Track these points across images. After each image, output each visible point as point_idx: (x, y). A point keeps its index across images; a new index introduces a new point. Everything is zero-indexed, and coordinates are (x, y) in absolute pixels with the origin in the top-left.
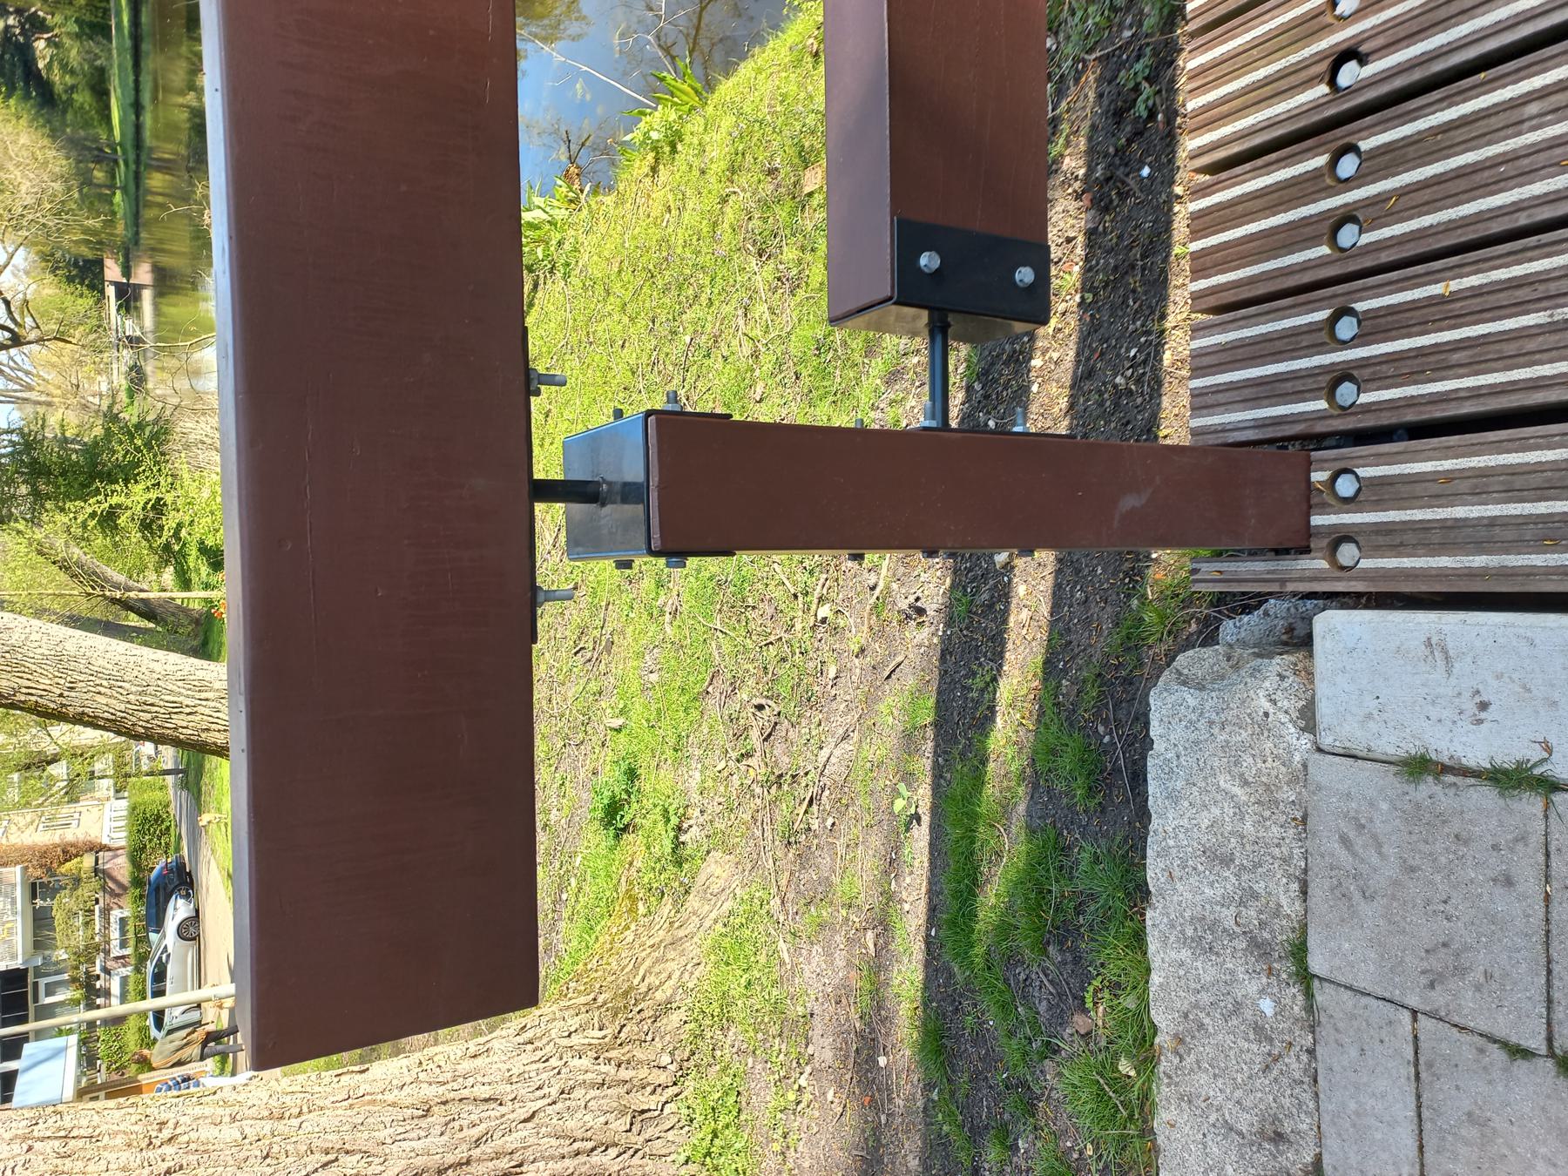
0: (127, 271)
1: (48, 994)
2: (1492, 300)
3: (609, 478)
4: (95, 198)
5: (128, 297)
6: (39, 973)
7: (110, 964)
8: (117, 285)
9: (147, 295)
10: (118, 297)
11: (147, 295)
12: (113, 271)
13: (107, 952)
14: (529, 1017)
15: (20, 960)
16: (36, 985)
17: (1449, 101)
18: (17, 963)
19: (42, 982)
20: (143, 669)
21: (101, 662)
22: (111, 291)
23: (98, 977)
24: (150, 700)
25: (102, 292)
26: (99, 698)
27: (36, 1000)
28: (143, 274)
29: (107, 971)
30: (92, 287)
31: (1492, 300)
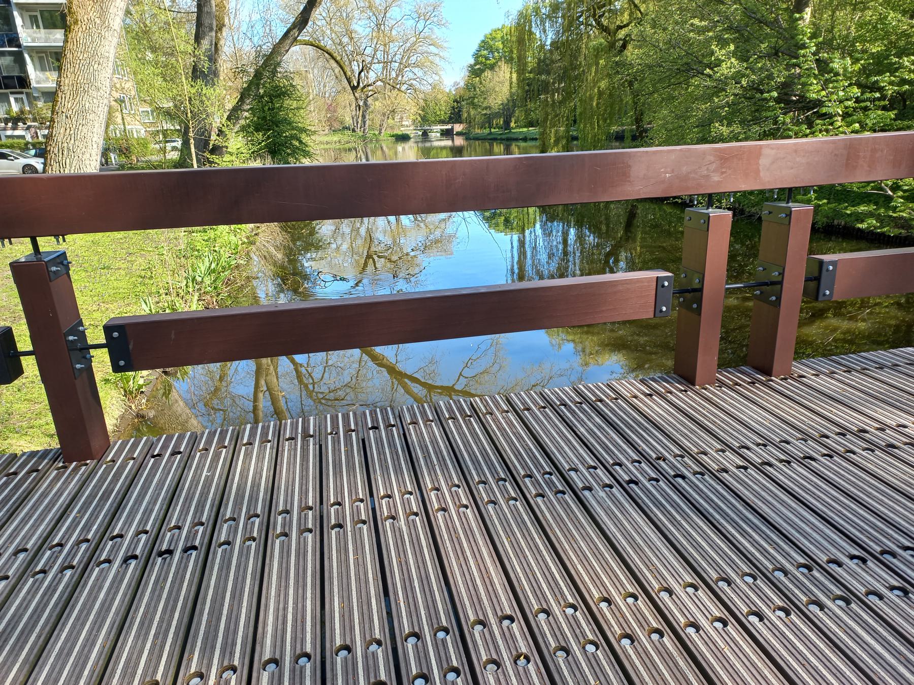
0: (459, 134)
1: (16, 99)
2: (178, 582)
3: (721, 312)
4: (488, 120)
5: (447, 134)
6: (28, 94)
7: (33, 130)
8: (452, 129)
9: (449, 143)
10: (447, 130)
11: (449, 143)
12: (458, 128)
13: (40, 129)
14: (13, 329)
15: (35, 85)
16: (22, 93)
17: (429, 545)
18: (34, 84)
19: (24, 97)
20: (84, 149)
21: (85, 131)
22: (449, 127)
23: (25, 124)
24: (65, 153)
25: (448, 123)
26: (62, 130)
27: (12, 93)
28: (459, 141)
29: (28, 128)
30: (450, 118)
31: (178, 582)
